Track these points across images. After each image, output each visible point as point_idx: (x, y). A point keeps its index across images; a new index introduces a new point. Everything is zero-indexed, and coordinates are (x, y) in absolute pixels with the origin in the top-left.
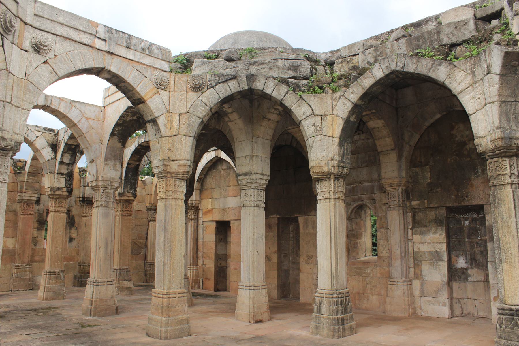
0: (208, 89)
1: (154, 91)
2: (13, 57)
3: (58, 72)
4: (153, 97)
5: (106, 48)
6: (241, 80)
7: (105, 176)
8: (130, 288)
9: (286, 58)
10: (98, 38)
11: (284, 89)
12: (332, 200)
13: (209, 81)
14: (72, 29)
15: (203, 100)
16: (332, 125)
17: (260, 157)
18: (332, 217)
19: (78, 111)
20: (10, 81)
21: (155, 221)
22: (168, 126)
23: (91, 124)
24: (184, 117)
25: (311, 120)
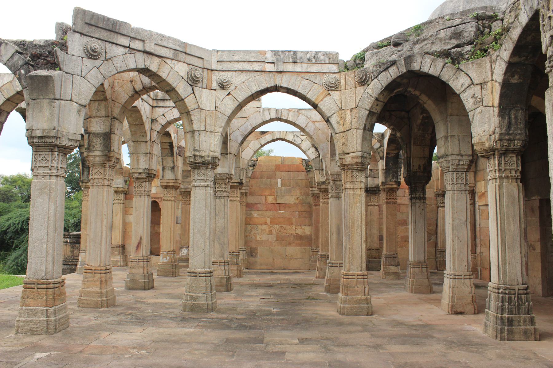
0: (372, 80)
1: (324, 94)
2: (204, 98)
3: (238, 99)
4: (324, 100)
5: (274, 69)
6: (400, 64)
7: (332, 170)
8: (397, 273)
9: (450, 26)
10: (267, 62)
11: (440, 63)
12: (498, 180)
13: (373, 73)
14: (246, 63)
15: (369, 93)
16: (492, 92)
17: (456, 137)
18: (498, 200)
19: (305, 117)
20: (203, 115)
21: (444, 207)
22: (341, 123)
23: (317, 126)
24: (354, 111)
25: (470, 92)
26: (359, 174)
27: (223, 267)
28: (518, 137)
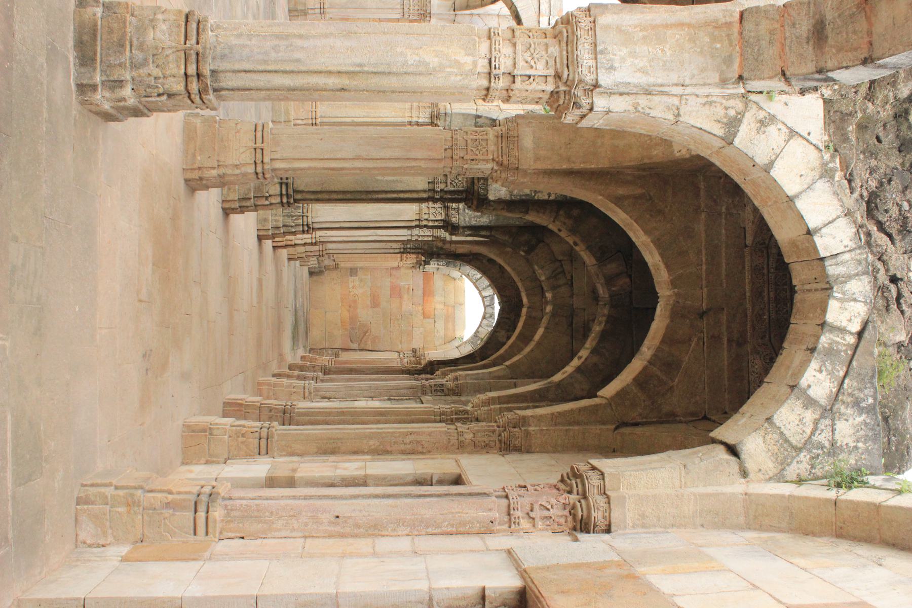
26: (428, 115)
27: (318, 6)
28: (462, 218)
